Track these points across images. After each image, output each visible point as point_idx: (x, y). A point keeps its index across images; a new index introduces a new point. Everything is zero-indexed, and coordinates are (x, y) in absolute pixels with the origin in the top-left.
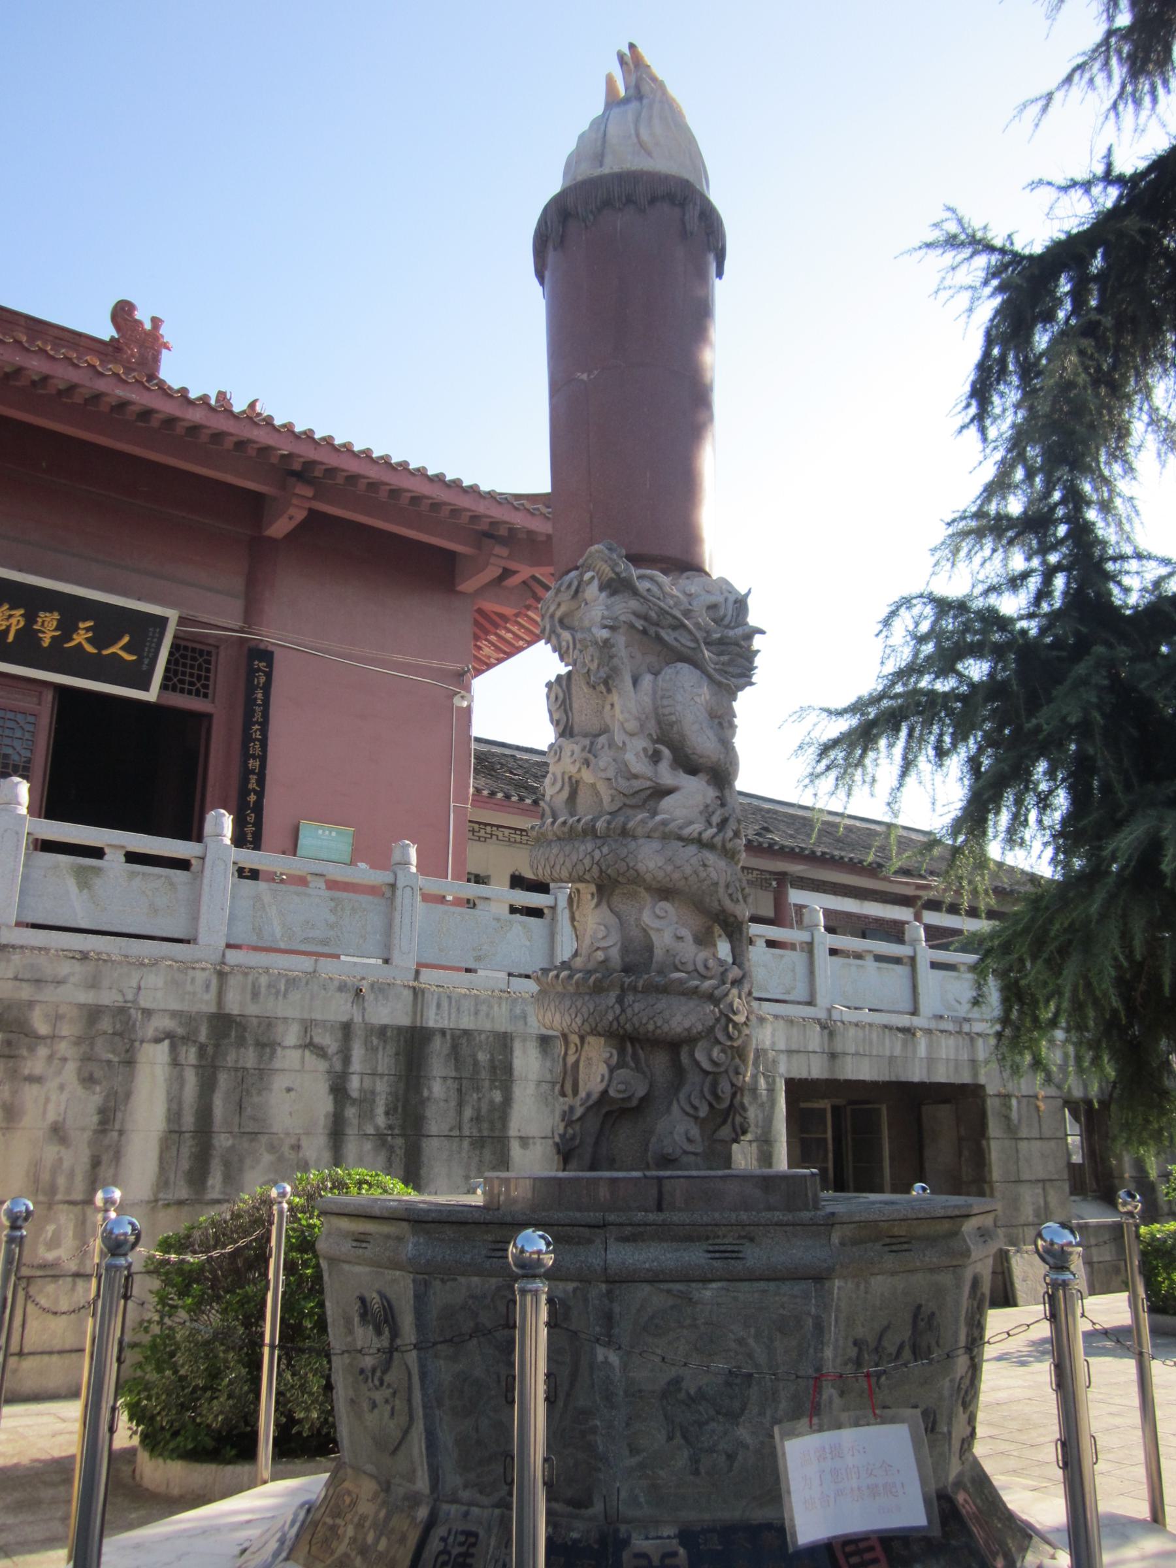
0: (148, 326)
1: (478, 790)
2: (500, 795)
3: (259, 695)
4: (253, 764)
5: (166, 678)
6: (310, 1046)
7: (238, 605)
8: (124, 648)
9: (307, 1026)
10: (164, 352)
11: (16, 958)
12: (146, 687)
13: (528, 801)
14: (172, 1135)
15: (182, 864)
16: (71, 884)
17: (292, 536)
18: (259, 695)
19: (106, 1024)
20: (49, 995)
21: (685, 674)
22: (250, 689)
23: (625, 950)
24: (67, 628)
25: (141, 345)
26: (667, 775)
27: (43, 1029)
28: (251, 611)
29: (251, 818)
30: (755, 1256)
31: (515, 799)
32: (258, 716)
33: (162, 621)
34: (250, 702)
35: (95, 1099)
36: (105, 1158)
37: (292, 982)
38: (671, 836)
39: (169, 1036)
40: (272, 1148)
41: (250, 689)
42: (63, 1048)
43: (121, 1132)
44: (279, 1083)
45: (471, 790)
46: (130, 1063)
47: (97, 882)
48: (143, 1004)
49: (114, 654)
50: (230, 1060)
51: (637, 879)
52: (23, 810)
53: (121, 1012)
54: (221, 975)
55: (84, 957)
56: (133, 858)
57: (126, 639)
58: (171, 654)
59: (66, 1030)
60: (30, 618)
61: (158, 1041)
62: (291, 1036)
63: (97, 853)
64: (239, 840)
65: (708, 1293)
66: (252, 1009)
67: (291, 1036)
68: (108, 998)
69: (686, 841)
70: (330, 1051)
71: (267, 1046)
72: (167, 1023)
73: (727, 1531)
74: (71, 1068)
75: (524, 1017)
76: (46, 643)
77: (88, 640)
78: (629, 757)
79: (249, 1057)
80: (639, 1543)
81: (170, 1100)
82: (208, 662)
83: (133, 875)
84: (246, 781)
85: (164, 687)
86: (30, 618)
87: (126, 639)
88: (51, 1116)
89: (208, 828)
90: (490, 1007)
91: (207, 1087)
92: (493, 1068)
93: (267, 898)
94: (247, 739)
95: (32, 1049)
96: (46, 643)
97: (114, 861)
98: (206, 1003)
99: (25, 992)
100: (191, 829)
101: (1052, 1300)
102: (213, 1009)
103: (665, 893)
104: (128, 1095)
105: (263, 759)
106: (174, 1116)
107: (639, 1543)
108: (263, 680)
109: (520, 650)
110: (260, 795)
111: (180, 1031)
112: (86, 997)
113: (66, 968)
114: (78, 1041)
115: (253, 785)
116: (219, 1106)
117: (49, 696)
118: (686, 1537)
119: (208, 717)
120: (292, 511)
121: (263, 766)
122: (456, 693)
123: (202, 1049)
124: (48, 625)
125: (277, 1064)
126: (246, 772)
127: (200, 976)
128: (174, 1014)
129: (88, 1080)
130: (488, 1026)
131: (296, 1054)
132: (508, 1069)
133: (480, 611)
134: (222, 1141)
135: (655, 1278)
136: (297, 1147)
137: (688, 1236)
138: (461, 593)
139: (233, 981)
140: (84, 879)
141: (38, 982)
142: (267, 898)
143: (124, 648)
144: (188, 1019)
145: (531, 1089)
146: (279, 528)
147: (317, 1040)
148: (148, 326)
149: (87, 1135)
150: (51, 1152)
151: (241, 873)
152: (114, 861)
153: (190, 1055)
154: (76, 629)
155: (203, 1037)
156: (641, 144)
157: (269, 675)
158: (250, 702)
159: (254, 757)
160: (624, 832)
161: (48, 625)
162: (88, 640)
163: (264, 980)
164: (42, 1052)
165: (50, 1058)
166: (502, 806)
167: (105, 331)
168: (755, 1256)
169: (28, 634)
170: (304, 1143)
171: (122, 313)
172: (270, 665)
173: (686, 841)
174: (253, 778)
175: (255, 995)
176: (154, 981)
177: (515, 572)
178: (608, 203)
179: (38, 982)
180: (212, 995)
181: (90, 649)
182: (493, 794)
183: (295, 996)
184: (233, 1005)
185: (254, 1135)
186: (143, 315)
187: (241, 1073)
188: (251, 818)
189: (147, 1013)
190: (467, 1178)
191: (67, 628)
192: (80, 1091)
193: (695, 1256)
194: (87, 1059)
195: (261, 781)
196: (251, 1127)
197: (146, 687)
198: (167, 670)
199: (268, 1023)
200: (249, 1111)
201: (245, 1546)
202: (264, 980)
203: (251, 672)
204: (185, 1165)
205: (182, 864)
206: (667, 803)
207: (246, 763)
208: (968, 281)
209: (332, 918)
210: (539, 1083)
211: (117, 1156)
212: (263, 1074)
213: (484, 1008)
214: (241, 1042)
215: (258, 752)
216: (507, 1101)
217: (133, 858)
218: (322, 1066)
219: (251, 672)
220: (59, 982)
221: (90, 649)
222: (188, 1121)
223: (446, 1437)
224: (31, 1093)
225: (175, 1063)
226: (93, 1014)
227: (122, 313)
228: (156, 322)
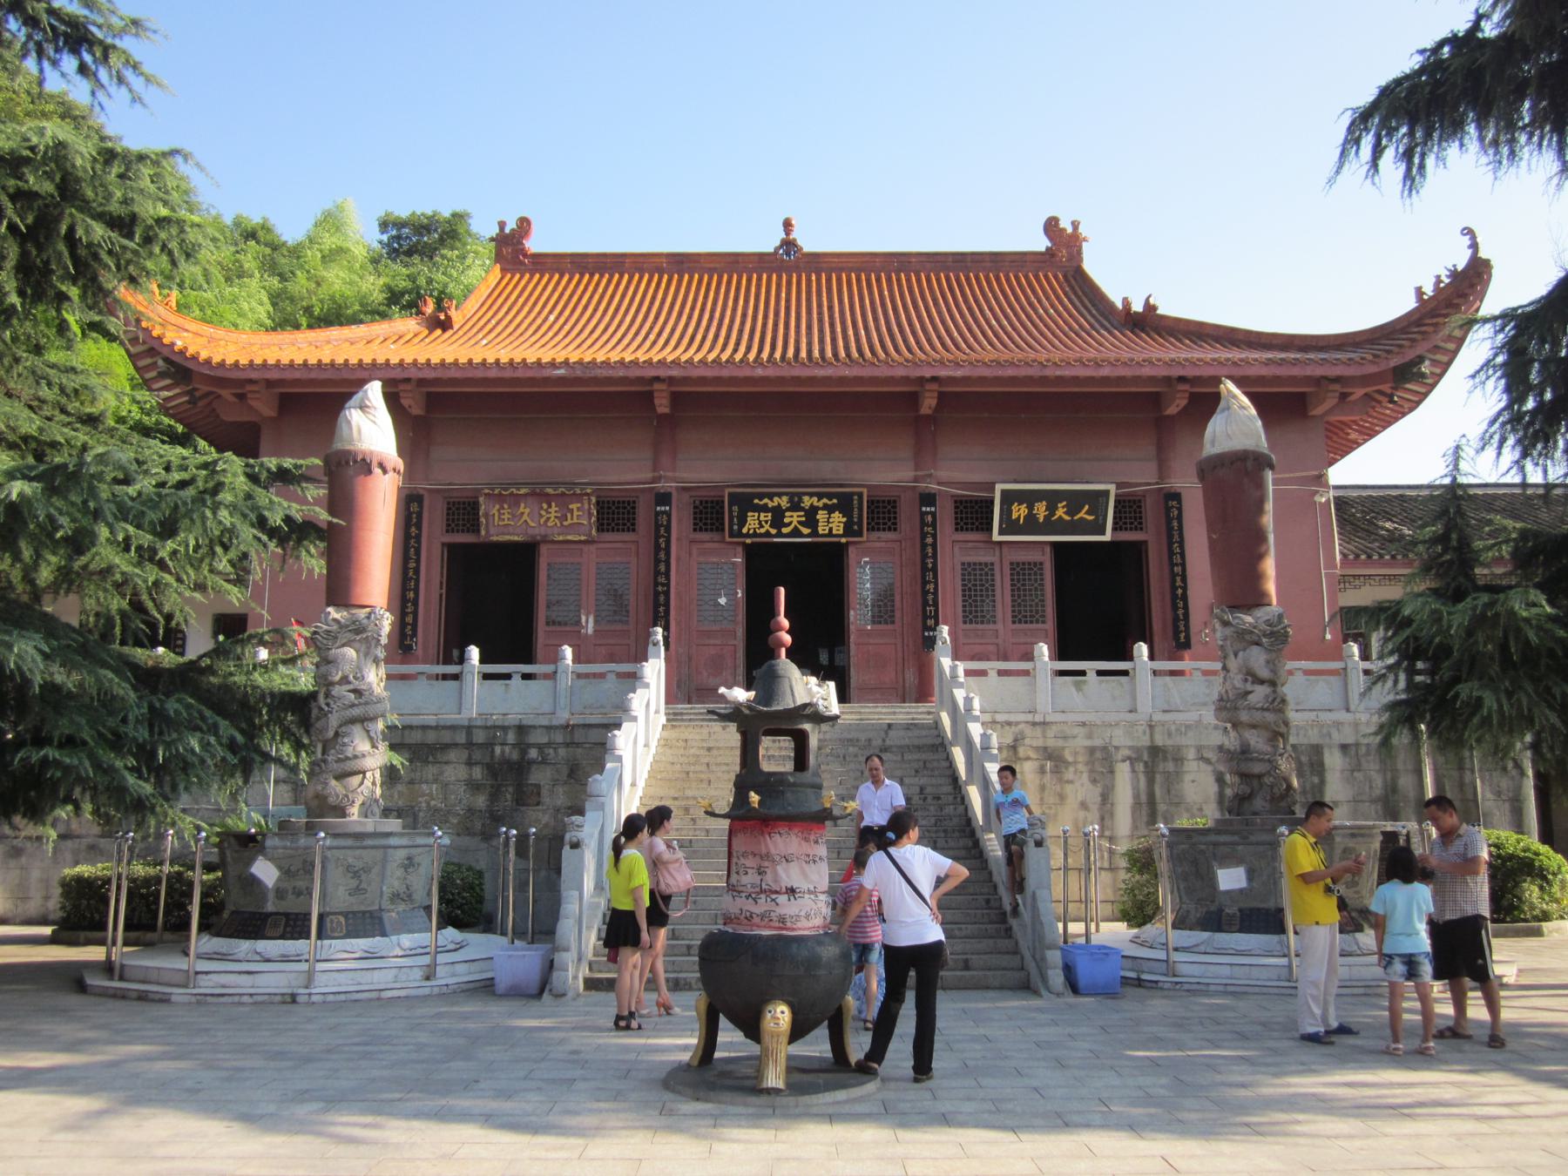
0: (1070, 230)
1: (1344, 556)
2: (1363, 557)
3: (1175, 524)
4: (1177, 569)
5: (1115, 523)
6: (1202, 758)
7: (1152, 467)
8: (1087, 513)
9: (1199, 749)
10: (1084, 244)
11: (1054, 727)
12: (1103, 533)
13: (1387, 557)
14: (1137, 805)
15: (1125, 673)
16: (1073, 689)
17: (1184, 411)
18: (1175, 524)
19: (1098, 755)
20: (1071, 743)
21: (1255, 650)
22: (1169, 520)
23: (1242, 746)
24: (1052, 509)
25: (1068, 247)
26: (1249, 687)
27: (1070, 759)
28: (1163, 471)
29: (1181, 604)
30: (1253, 838)
31: (1376, 557)
32: (1176, 538)
33: (1107, 493)
34: (1170, 529)
35: (1098, 790)
36: (1106, 817)
37: (1188, 727)
38: (1250, 708)
39: (1129, 758)
40: (1187, 810)
41: (1169, 520)
42: (1081, 767)
43: (1112, 804)
44: (1187, 778)
45: (1338, 557)
46: (1112, 772)
47: (1085, 687)
48: (1115, 743)
49: (1082, 518)
50: (1161, 767)
51: (1241, 723)
52: (1046, 659)
53: (1104, 749)
54: (1151, 727)
55: (1084, 724)
56: (1100, 673)
57: (1087, 507)
58: (1115, 507)
59: (1080, 759)
60: (1030, 508)
61: (1124, 761)
62: (1191, 754)
63: (1082, 673)
64: (1152, 657)
65: (1240, 848)
66: (1169, 742)
67: (1191, 754)
68: (1098, 742)
69: (1257, 709)
70: (1214, 760)
71: (1179, 760)
72: (1127, 752)
73: (1251, 910)
74: (1085, 776)
75: (1330, 735)
76: (1041, 520)
77: (1065, 513)
78: (1236, 682)
79: (1170, 766)
80: (1227, 911)
81: (1133, 789)
82: (1140, 507)
83: (1104, 685)
84: (1173, 581)
85: (1114, 529)
86: (1030, 508)
87: (1087, 507)
88: (1080, 799)
89: (1135, 653)
90: (1306, 730)
91: (1151, 782)
92: (1312, 765)
93: (1171, 685)
94: (1171, 553)
95: (1066, 768)
96: (1041, 520)
97: (1091, 676)
98: (1145, 741)
99: (1060, 743)
100: (1127, 655)
101: (1102, 819)
102: (1148, 744)
103: (1254, 727)
104: (1113, 786)
105: (1183, 565)
106: (1136, 796)
107: (1227, 911)
108: (1176, 512)
109: (1378, 433)
110: (1185, 589)
111: (1134, 756)
112: (1088, 743)
113: (1076, 730)
114: (1087, 764)
115: (1179, 583)
116: (1158, 791)
117: (1048, 549)
118: (1240, 910)
119: (1145, 542)
120: (1178, 401)
121: (1184, 570)
122: (1317, 492)
123: (1146, 763)
124: (1041, 510)
125: (1185, 769)
126: (1173, 576)
127: (1141, 729)
128: (1130, 748)
129: (1094, 781)
130: (1306, 741)
131: (1195, 764)
132: (1321, 764)
133: (1327, 422)
134: (1161, 807)
135: (1224, 844)
136: (1201, 810)
137: (1233, 833)
138: (1313, 416)
139: (1158, 730)
140: (1078, 686)
141: (1065, 738)
142: (1171, 685)
143: (1087, 513)
144: (1137, 750)
145: (1338, 774)
146: (1172, 410)
147: (1205, 755)
148: (1070, 230)
149: (1097, 806)
150: (1082, 814)
151: (1155, 673)
152: (1091, 676)
153: (1140, 767)
154: (1057, 508)
155: (1146, 757)
156: (1228, 435)
157: (1180, 509)
158: (1170, 529)
159: (1177, 565)
160: (1236, 708)
161: (1041, 510)
162: (1065, 513)
163: (1173, 728)
164: (1071, 769)
165: (1075, 772)
166: (1365, 565)
167: (1041, 244)
168: (1253, 838)
169: (1031, 517)
170: (1204, 807)
171: (1051, 226)
172: (1180, 502)
173: (1257, 709)
174: (1178, 579)
175: (1170, 735)
176: (1118, 732)
177: (1351, 394)
178: (1215, 467)
179: (1065, 738)
180: (1147, 737)
181: (1067, 518)
182: (1357, 556)
183: (1190, 734)
184: (1159, 741)
185: (1178, 804)
186: (1065, 224)
187: (1167, 774)
188: (1181, 604)
189: (1117, 748)
190: (222, 776)
191: (1052, 509)
192: (1091, 787)
193: (1236, 838)
194: (1091, 771)
195: (1184, 579)
196: (1176, 800)
197: (1103, 533)
198: (1115, 518)
199: (1179, 748)
200: (1173, 792)
201: (1018, 776)
202: (1173, 728)
203: (1168, 510)
204: (1145, 819)
205: (1125, 673)
206: (1250, 697)
207: (1172, 571)
208: (1487, 335)
209: (1207, 691)
210: (1342, 771)
211: (1112, 815)
212: (1178, 774)
213: (1302, 732)
214: (1165, 759)
215: (1179, 561)
216: (1323, 782)
217: (1100, 673)
218: (1210, 768)
219: (1168, 510)
220: (1074, 737)
221: (1067, 518)
222: (1144, 798)
223: (1182, 887)
224: (1069, 789)
225: (1133, 771)
226: (1092, 750)
227: (1051, 226)
228: (1075, 225)
